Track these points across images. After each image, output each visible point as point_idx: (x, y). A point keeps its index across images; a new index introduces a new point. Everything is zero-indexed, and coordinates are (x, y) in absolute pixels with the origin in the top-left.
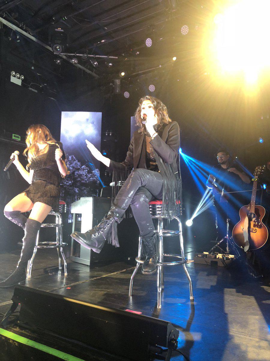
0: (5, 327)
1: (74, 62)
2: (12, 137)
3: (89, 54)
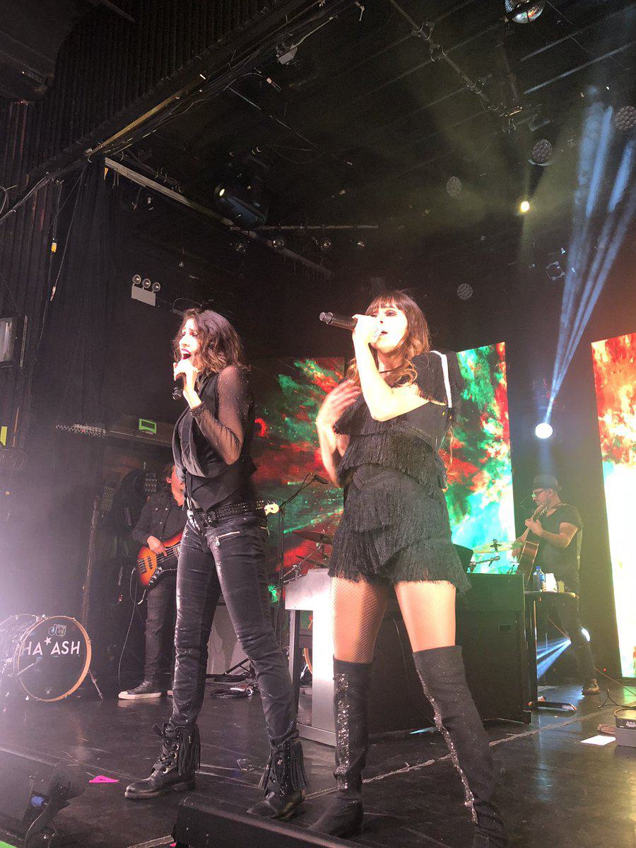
0: (353, 325)
1: (276, 244)
2: (138, 428)
3: (310, 225)
